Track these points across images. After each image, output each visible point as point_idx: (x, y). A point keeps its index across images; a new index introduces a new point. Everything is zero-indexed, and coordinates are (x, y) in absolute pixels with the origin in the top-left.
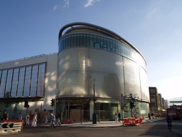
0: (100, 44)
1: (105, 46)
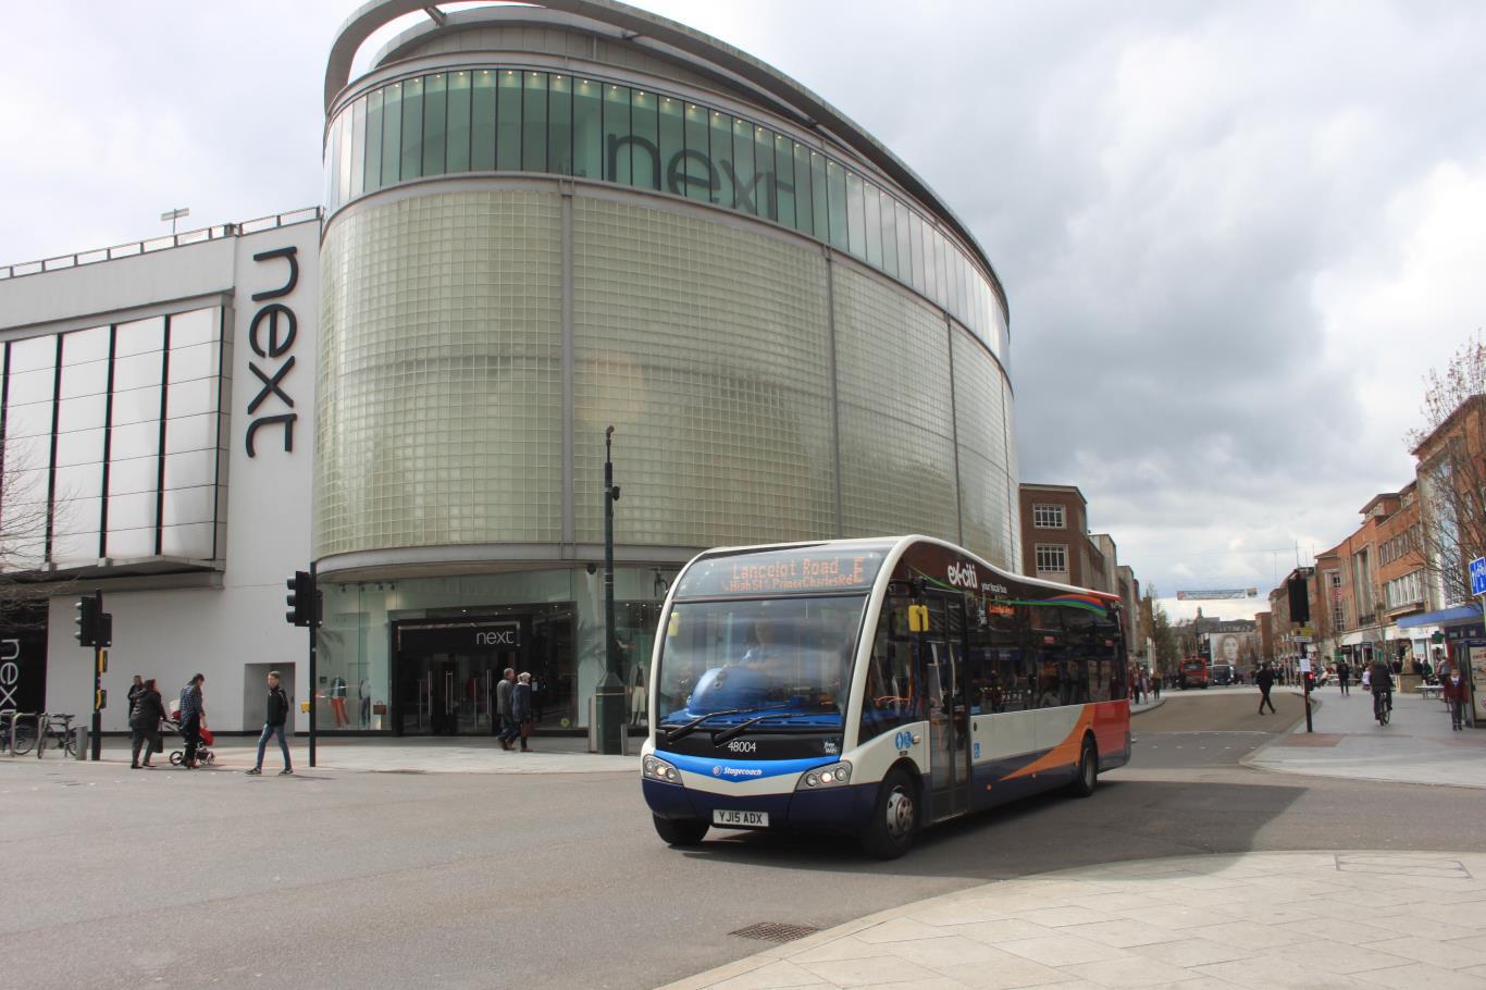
0: (655, 154)
1: (695, 169)
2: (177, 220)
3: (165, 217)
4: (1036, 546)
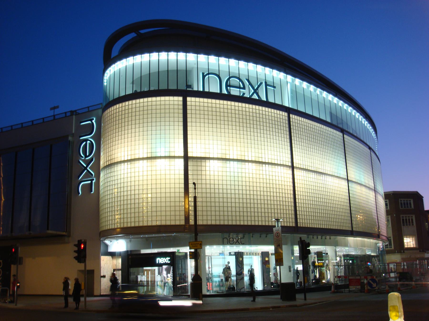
2: (55, 110)
3: (51, 109)
4: (401, 216)
